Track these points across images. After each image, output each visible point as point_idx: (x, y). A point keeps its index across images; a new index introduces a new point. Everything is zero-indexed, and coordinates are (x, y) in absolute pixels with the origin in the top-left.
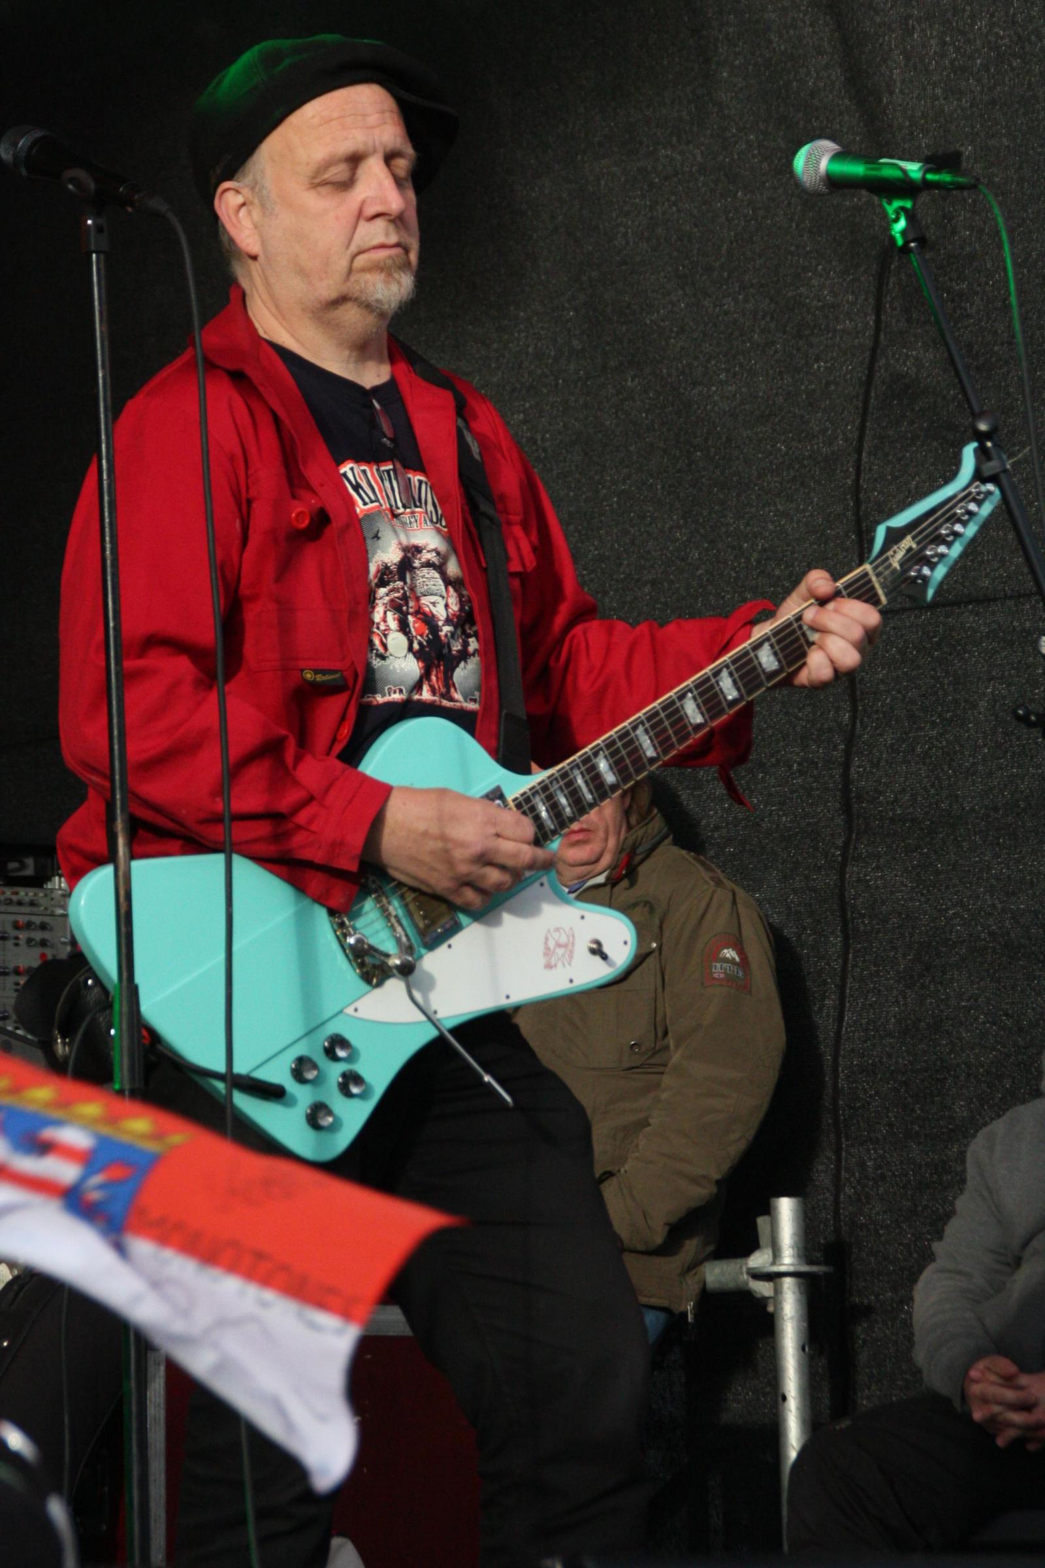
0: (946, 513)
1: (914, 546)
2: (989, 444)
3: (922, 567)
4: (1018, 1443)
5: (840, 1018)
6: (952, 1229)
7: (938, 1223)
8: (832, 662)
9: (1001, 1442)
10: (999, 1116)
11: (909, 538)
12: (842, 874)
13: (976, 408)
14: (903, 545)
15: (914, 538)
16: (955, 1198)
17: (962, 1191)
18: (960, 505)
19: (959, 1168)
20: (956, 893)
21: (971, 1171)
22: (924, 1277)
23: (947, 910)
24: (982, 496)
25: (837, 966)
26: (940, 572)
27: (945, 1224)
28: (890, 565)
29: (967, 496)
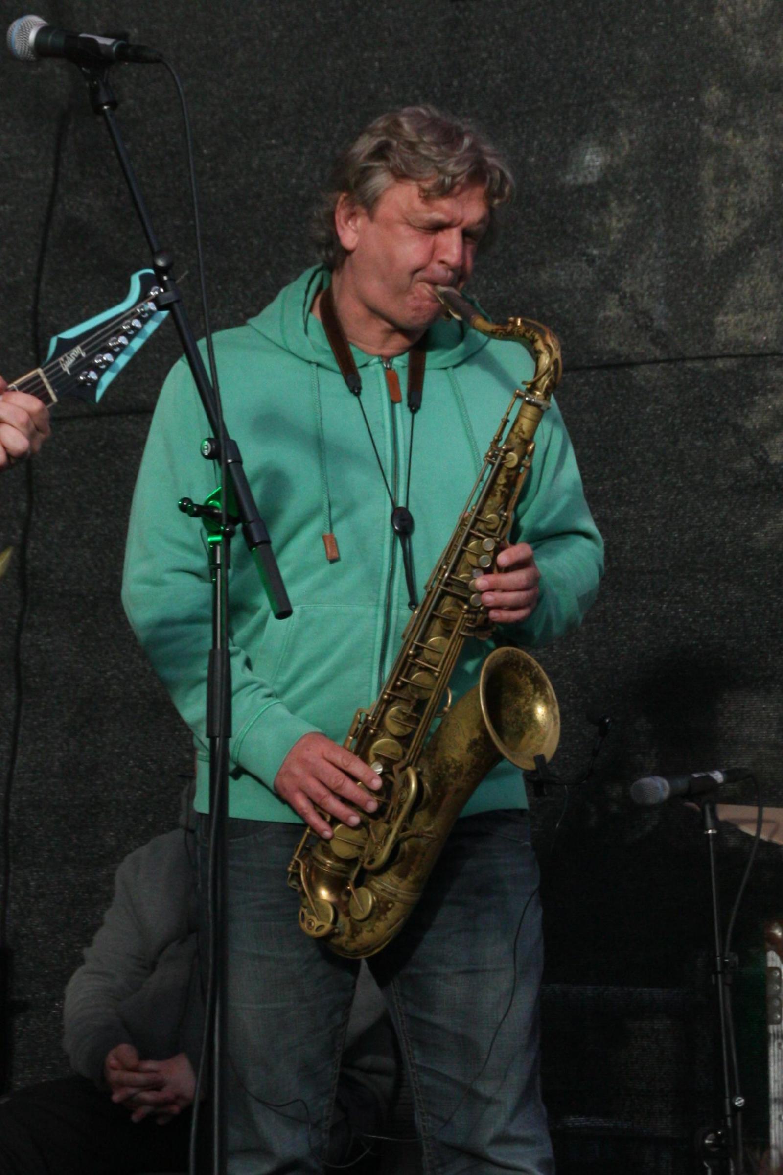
0: (114, 327)
1: (84, 355)
2: (165, 278)
3: (89, 372)
4: (149, 1119)
5: (13, 761)
6: (102, 936)
7: (87, 936)
8: (5, 448)
9: (135, 1118)
10: (142, 845)
11: (78, 348)
12: (17, 640)
13: (156, 248)
14: (73, 354)
15: (82, 348)
16: (102, 913)
17: (108, 907)
18: (126, 322)
19: (107, 888)
20: (114, 658)
21: (119, 887)
22: (74, 978)
23: (105, 672)
24: (146, 315)
25: (11, 717)
26: (108, 378)
27: (93, 935)
28: (61, 369)
29: (131, 314)
